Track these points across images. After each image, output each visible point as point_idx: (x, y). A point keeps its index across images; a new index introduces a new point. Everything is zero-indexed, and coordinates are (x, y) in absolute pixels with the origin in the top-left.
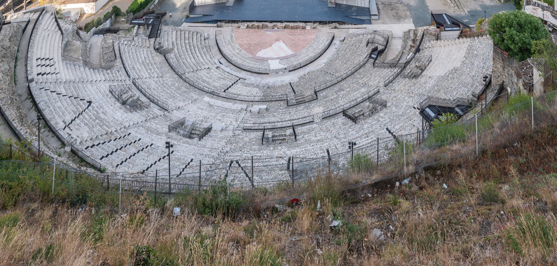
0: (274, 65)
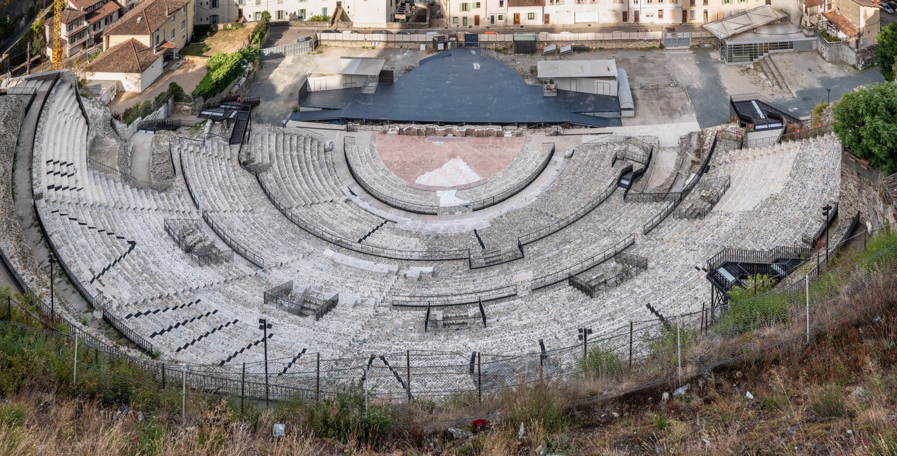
0: (447, 199)
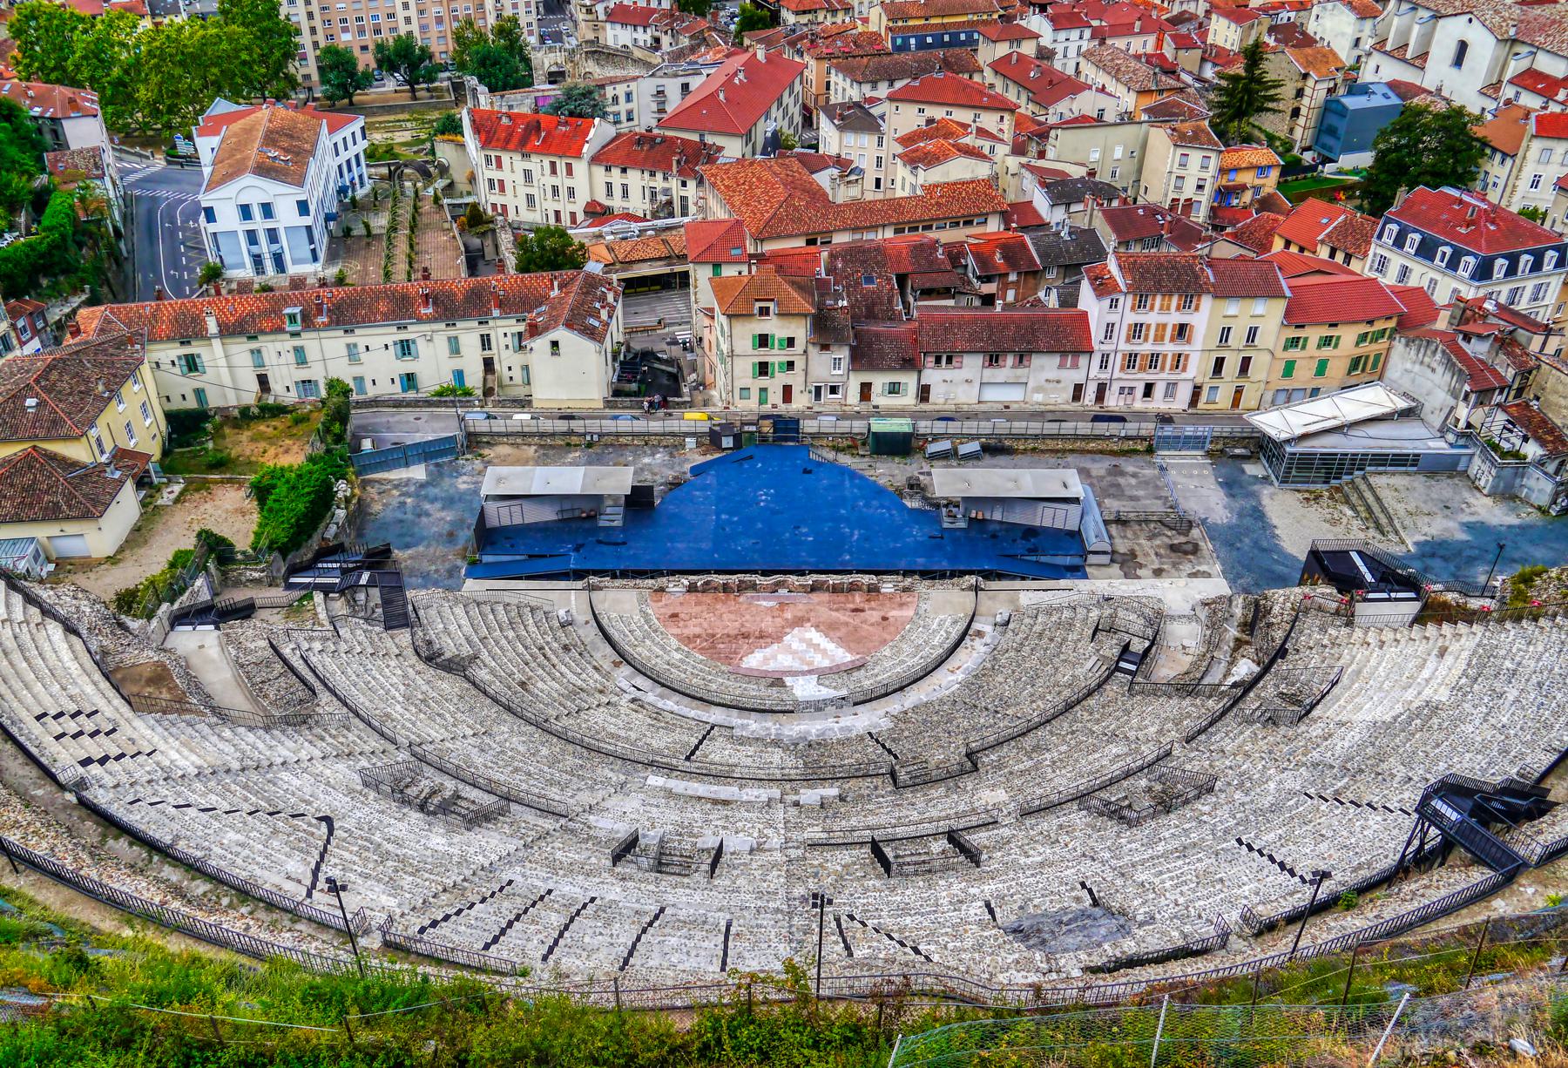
0: (805, 689)
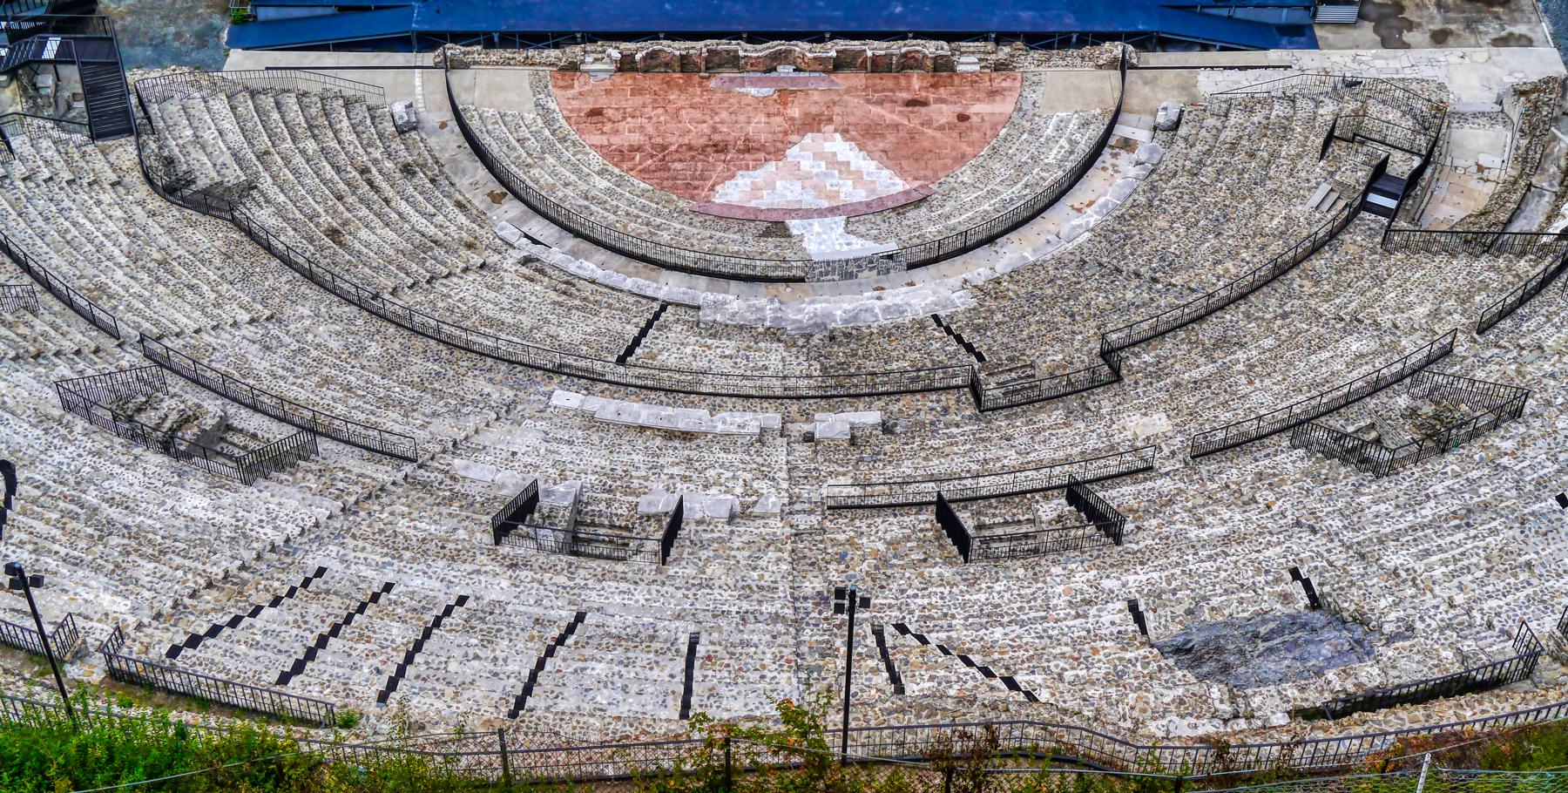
0: (824, 240)
